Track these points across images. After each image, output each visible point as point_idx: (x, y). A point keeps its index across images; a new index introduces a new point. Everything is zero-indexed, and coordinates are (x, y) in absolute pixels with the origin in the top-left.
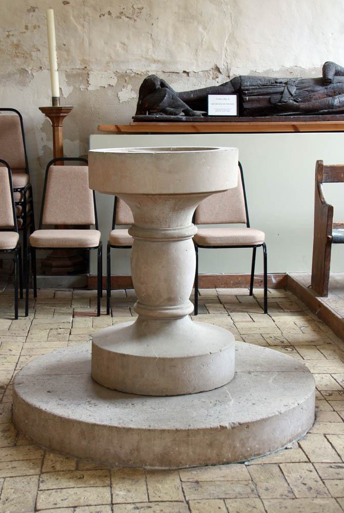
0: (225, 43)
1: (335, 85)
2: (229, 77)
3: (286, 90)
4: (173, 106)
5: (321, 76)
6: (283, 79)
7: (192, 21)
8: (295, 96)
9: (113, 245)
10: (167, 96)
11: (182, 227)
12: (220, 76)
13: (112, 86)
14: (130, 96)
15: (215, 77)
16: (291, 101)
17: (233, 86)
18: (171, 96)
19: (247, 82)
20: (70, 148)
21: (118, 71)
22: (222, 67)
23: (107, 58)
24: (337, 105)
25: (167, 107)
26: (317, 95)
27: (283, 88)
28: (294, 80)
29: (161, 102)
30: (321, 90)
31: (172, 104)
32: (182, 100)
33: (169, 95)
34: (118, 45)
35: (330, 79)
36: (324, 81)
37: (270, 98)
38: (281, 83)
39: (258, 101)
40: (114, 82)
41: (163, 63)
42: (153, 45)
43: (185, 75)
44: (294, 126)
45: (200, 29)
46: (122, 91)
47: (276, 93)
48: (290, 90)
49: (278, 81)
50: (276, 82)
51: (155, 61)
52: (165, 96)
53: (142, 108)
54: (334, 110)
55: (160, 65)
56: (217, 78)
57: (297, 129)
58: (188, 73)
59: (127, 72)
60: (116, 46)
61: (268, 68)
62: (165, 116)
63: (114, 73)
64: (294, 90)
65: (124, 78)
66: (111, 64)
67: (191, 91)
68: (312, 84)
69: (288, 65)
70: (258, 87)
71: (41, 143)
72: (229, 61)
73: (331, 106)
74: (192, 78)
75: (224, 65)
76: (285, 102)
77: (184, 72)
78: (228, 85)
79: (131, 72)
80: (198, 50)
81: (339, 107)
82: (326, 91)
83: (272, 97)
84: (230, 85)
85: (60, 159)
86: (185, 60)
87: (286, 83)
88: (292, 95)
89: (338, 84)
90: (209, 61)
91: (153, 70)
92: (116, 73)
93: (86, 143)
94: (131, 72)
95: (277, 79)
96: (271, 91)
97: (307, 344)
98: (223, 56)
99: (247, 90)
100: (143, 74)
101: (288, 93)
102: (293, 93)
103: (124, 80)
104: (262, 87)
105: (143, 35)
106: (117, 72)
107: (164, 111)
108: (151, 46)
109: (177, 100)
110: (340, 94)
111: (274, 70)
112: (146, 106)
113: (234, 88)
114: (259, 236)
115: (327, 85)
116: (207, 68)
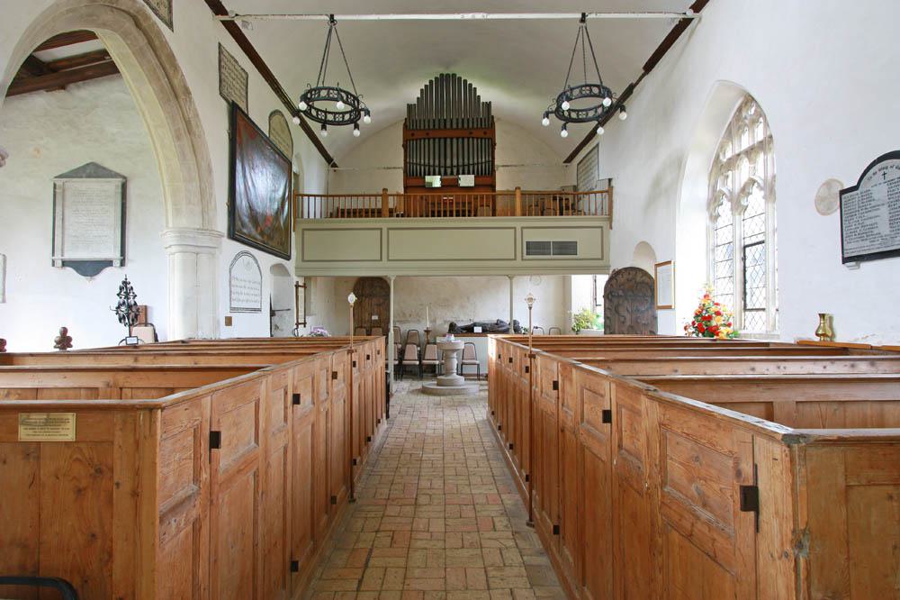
9: (442, 364)
11: (526, 400)
14: (447, 327)
20: (432, 340)
36: (497, 324)
65: (445, 322)
71: (424, 339)
85: (428, 343)
86: (462, 317)
91: (453, 320)
93: (435, 339)
97: (190, 156)
114: (478, 362)
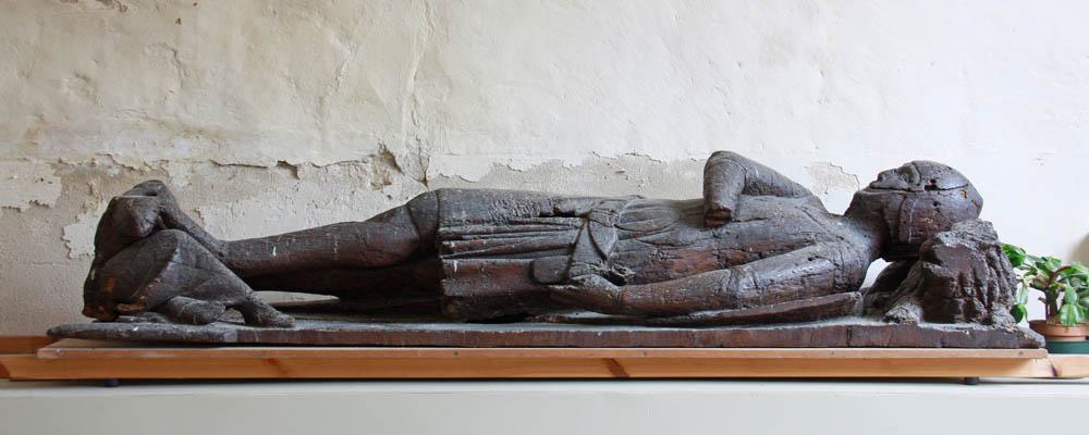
0: (411, 80)
1: (744, 226)
2: (425, 181)
3: (585, 241)
4: (200, 289)
5: (699, 195)
6: (580, 199)
7: (304, 14)
8: (614, 259)
10: (176, 257)
12: (395, 177)
13: (46, 206)
15: (381, 181)
16: (597, 280)
17: (414, 222)
18: (194, 258)
19: (459, 210)
21: (64, 159)
22: (401, 153)
23: (30, 121)
24: (747, 296)
25: (177, 294)
26: (685, 259)
27: (575, 233)
28: (611, 206)
29: (151, 280)
30: (698, 239)
31: (196, 284)
32: (230, 265)
33: (185, 257)
34: (66, 81)
35: (725, 210)
36: (706, 214)
37: (532, 264)
38: (571, 214)
39: (494, 273)
40: (51, 193)
41: (217, 136)
42: (182, 83)
43: (287, 172)
44: (612, 364)
45: (332, 38)
46: (77, 220)
47: (553, 248)
48: (598, 240)
49: (564, 207)
50: (559, 212)
51: (187, 132)
52: (169, 259)
53: (103, 296)
54: (741, 312)
55: (205, 143)
56: (388, 183)
57: (622, 371)
58: (294, 169)
59: (97, 162)
60: (57, 84)
61: (547, 158)
62: (166, 327)
63: (53, 166)
64: (610, 241)
66: (41, 139)
67: (273, 239)
68: (669, 221)
69: (611, 148)
70: (492, 228)
72: (424, 134)
73: (730, 300)
74: (307, 186)
75: (408, 146)
76: (576, 283)
77: (283, 164)
78: (398, 220)
79: (108, 162)
80: (327, 99)
81: (755, 301)
82: (714, 244)
83: (538, 262)
84: (404, 217)
87: (585, 216)
88: (604, 257)
89: (754, 224)
90: (360, 132)
92: (59, 165)
94: (108, 162)
95: (559, 200)
96: (535, 240)
98: (406, 119)
99: (458, 237)
100: (148, 169)
101: (591, 251)
102: (607, 249)
103: (88, 190)
104: (505, 227)
105: (147, 51)
106: (60, 161)
107: (164, 308)
108: (175, 86)
109: (212, 271)
110: (762, 256)
111: (566, 165)
112: (109, 289)
113: (417, 229)
115: (716, 227)
116: (356, 155)
